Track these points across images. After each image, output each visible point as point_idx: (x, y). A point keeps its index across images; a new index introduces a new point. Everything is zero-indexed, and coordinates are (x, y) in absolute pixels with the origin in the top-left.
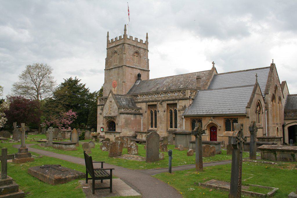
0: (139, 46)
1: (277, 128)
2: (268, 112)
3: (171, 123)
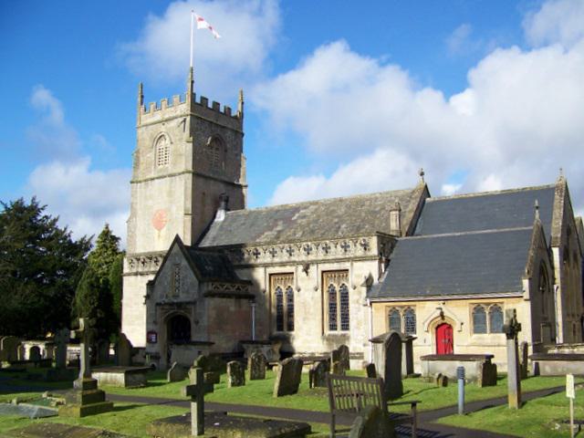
1: (574, 325)
3: (333, 318)
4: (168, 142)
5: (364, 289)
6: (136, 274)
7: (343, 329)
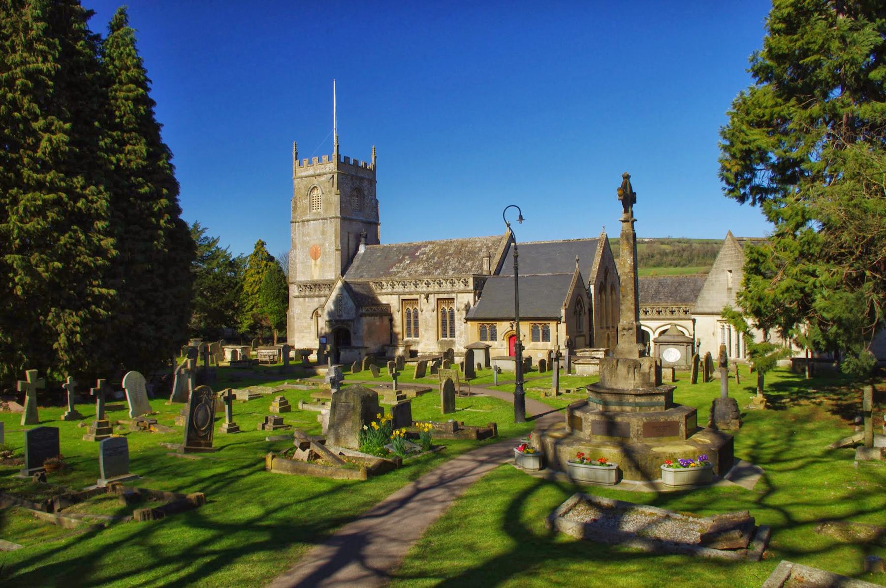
0: (361, 175)
1: (608, 334)
3: (444, 329)
4: (319, 192)
5: (464, 312)
6: (304, 297)
7: (451, 337)
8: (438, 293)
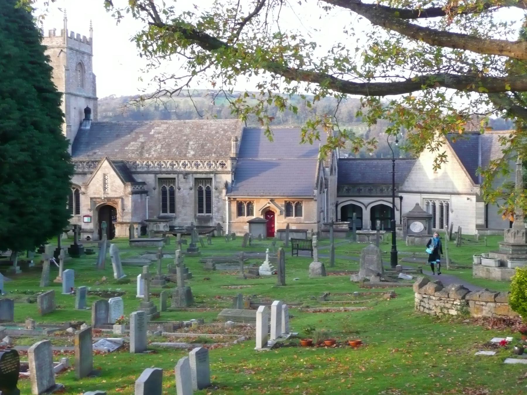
2: (327, 190)
7: (207, 212)
8: (196, 173)
